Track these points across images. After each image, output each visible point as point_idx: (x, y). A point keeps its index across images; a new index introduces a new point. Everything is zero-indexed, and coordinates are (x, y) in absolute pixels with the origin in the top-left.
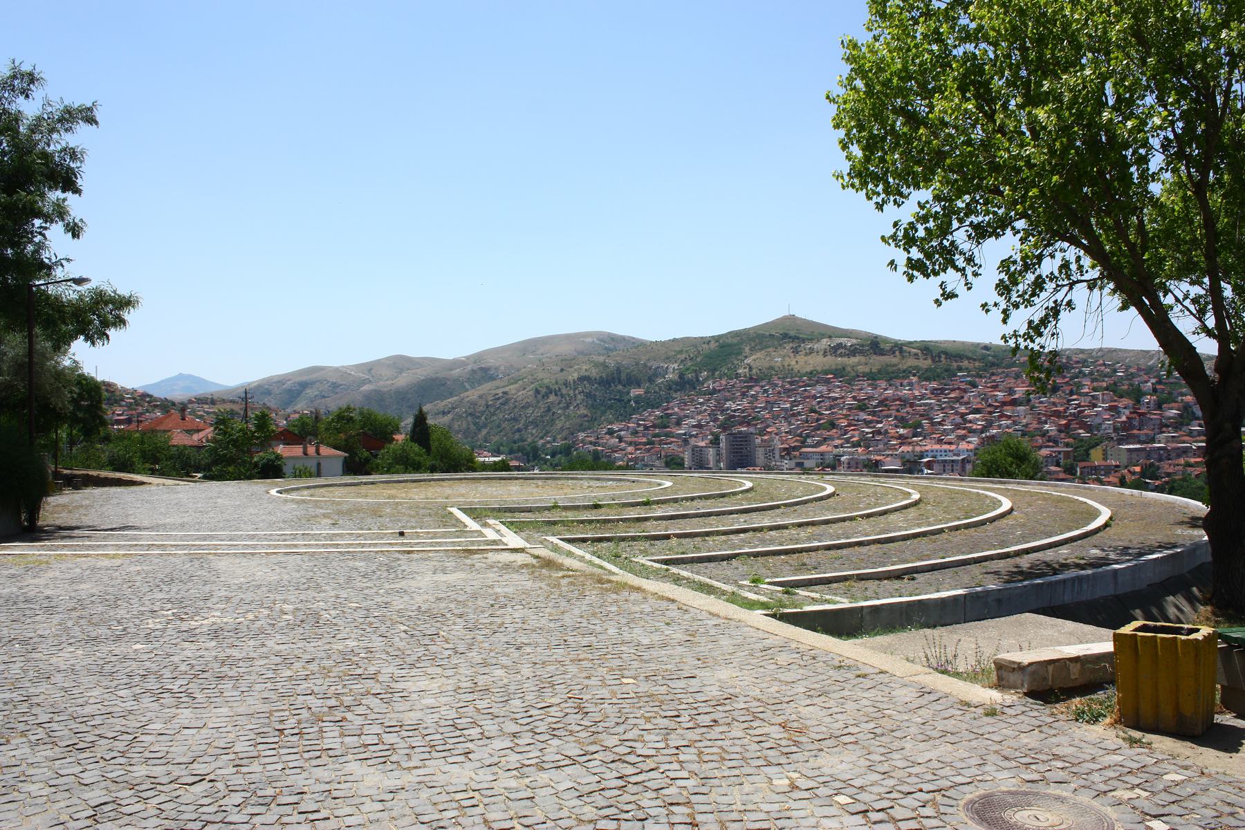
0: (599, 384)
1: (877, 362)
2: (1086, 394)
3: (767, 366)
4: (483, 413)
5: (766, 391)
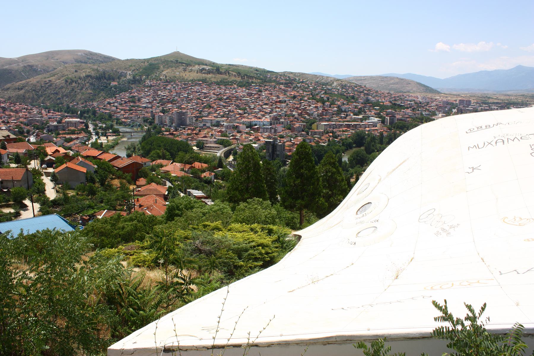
0: (96, 79)
1: (219, 77)
2: (306, 101)
3: (173, 76)
4: (40, 90)
5: (174, 87)
